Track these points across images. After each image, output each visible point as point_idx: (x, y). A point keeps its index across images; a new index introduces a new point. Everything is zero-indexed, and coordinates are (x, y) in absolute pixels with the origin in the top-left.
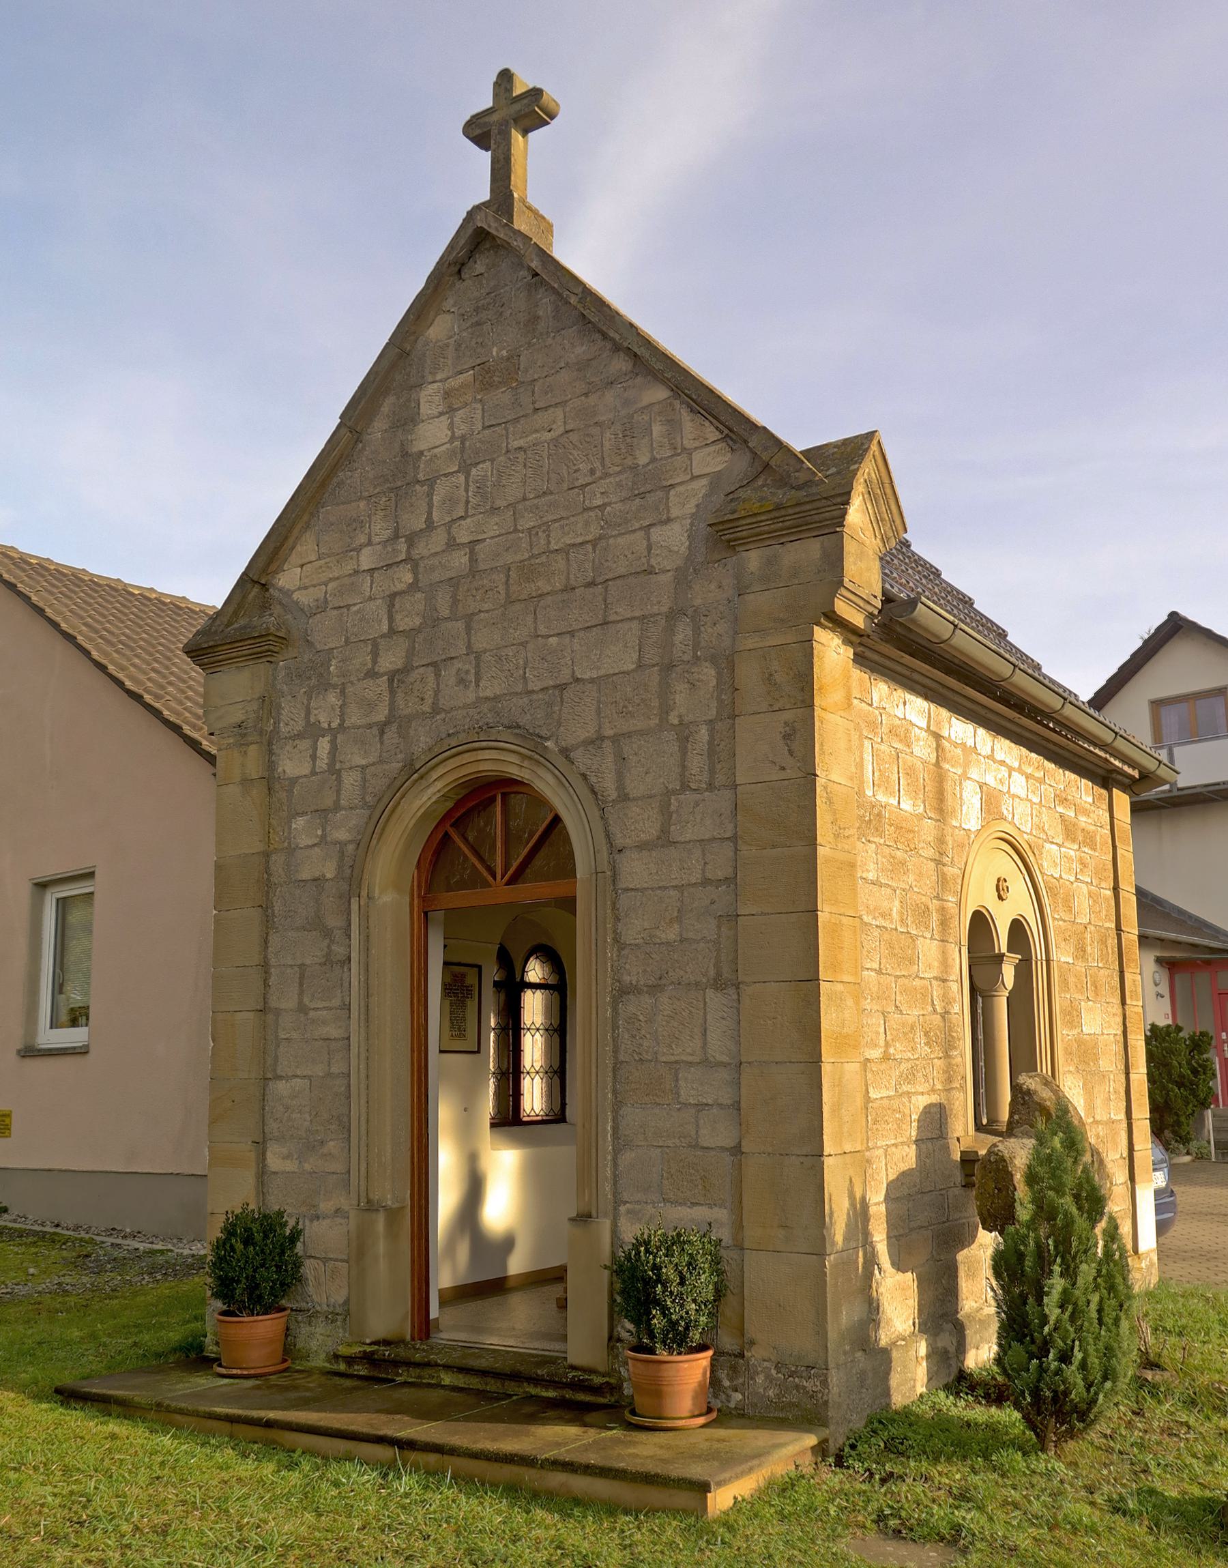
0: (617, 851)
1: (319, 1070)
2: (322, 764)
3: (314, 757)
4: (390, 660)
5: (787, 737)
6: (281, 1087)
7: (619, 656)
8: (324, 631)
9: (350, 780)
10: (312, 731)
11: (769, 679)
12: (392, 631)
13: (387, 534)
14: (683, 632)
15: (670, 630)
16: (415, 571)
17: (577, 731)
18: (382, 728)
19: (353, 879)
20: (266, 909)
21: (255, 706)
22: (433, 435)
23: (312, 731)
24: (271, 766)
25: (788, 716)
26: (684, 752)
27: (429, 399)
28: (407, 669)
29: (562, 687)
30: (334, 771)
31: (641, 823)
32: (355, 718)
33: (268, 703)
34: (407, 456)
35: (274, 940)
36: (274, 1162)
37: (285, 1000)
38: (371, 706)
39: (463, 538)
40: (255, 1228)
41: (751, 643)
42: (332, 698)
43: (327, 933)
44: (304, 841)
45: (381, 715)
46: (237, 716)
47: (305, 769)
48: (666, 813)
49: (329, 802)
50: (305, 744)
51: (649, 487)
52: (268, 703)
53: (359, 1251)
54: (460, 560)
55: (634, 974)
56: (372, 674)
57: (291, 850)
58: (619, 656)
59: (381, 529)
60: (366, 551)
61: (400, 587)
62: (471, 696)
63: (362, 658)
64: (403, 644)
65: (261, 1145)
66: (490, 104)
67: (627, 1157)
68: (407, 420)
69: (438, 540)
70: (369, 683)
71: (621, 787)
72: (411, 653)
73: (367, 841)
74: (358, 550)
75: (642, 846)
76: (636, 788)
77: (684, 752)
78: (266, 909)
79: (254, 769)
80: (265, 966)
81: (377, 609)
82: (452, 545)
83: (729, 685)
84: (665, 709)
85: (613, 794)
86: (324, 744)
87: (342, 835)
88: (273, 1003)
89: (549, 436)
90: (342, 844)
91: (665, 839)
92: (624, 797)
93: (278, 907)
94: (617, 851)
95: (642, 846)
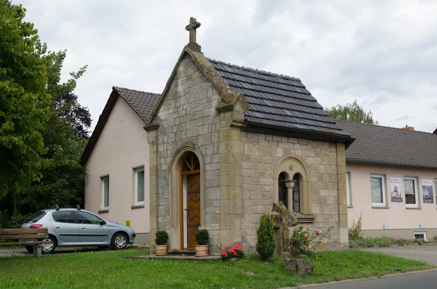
0: (205, 164)
1: (165, 204)
2: (165, 149)
3: (164, 148)
4: (175, 130)
5: (226, 145)
6: (160, 207)
7: (205, 131)
8: (165, 124)
9: (169, 151)
10: (164, 143)
11: (224, 136)
12: (175, 125)
13: (174, 107)
14: (214, 126)
15: (212, 126)
16: (178, 114)
17: (200, 144)
18: (174, 142)
19: (170, 170)
20: (157, 175)
21: (155, 138)
22: (180, 88)
23: (164, 143)
24: (157, 149)
25: (226, 142)
26: (214, 147)
27: (180, 82)
28: (177, 132)
29: (198, 136)
30: (167, 150)
31: (208, 160)
32: (170, 141)
33: (157, 137)
34: (177, 92)
35: (159, 180)
36: (160, 221)
37: (160, 191)
38: (172, 138)
39: (185, 108)
40: (270, 218)
41: (222, 129)
42: (166, 137)
43: (166, 180)
44: (163, 163)
45: (173, 140)
46: (152, 140)
47: (162, 150)
48: (211, 158)
49: (166, 156)
50: (163, 145)
51: (210, 101)
52: (157, 137)
53: (279, 242)
54: (184, 112)
55: (208, 186)
56: (172, 133)
57: (161, 165)
58: (205, 131)
59: (173, 106)
60: (171, 110)
61: (176, 117)
62: (186, 137)
63: (171, 130)
64: (176, 127)
65: (157, 217)
66: (189, 24)
67: (207, 216)
68: (176, 86)
69: (181, 108)
70: (172, 134)
71: (206, 154)
72: (177, 129)
73: (172, 165)
74: (170, 109)
75: (209, 164)
76: (208, 154)
77: (214, 147)
78: (157, 175)
79: (155, 150)
80: (157, 185)
81: (172, 121)
82: (183, 109)
83: (219, 137)
84: (211, 140)
85: (205, 155)
86: (165, 145)
87: (168, 162)
88: (159, 192)
89: (196, 90)
90: (168, 163)
91: (211, 163)
92: (206, 155)
93: (159, 175)
94: (205, 164)
95: (209, 164)
